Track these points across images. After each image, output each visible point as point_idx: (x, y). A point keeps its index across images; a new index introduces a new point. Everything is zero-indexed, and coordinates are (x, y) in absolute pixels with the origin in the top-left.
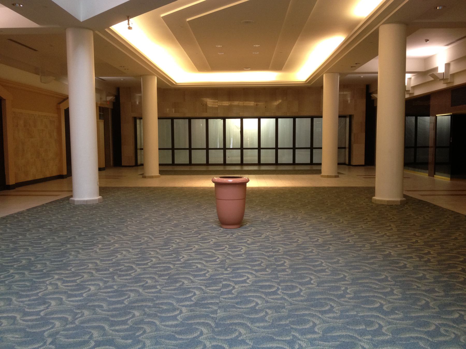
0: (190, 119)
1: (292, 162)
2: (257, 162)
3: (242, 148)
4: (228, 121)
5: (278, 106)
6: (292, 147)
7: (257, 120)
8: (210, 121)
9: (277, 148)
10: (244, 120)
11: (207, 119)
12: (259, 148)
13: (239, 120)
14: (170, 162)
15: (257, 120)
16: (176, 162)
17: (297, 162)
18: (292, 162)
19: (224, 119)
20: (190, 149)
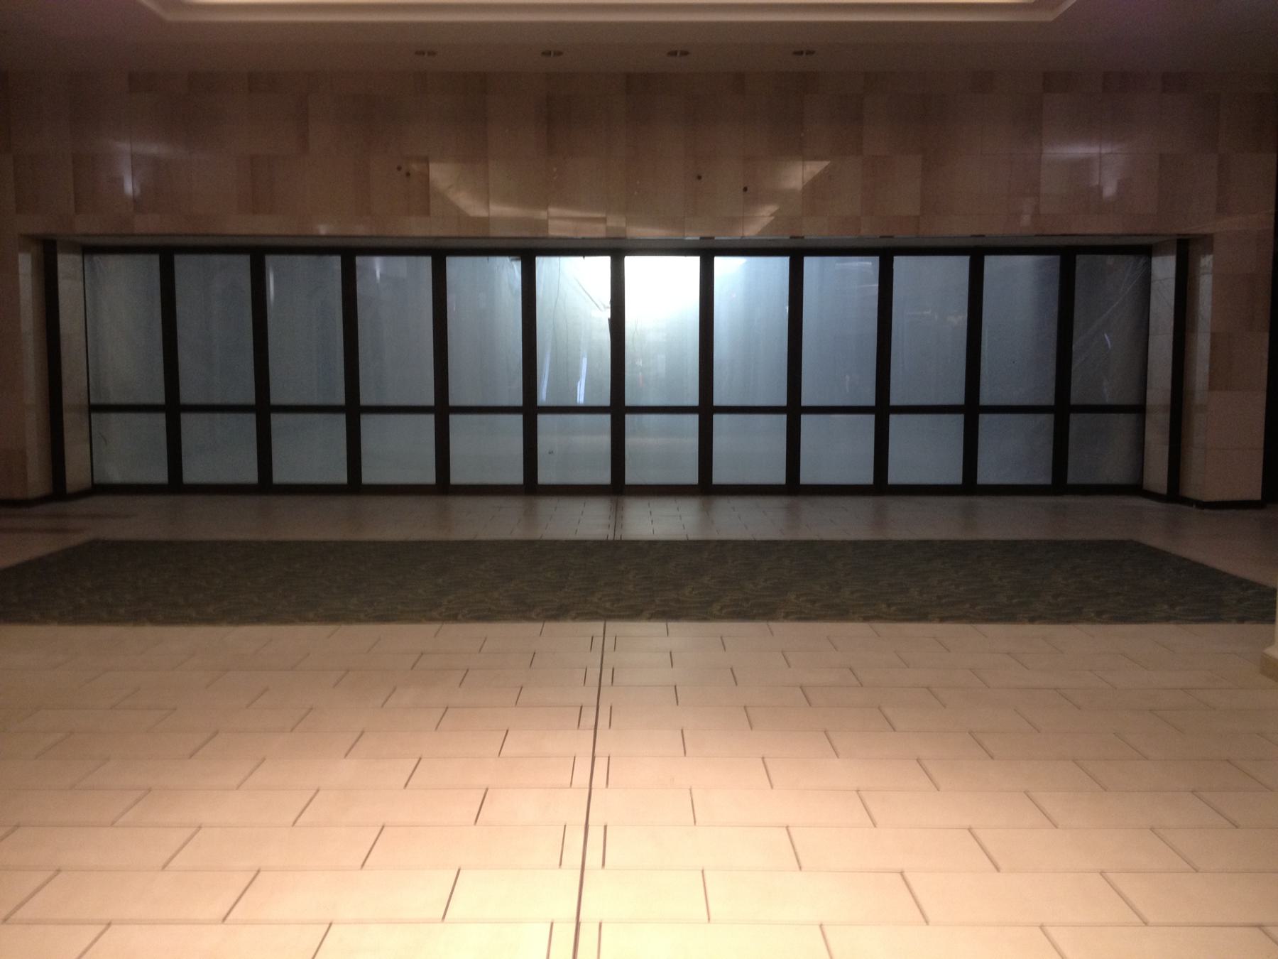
0: (349, 254)
1: (177, 258)
2: (692, 477)
3: (618, 409)
4: (544, 265)
5: (814, 188)
6: (870, 401)
7: (694, 262)
8: (455, 266)
9: (794, 410)
10: (630, 262)
11: (439, 255)
12: (706, 409)
13: (605, 262)
14: (250, 475)
15: (694, 262)
16: (279, 477)
17: (894, 477)
18: (177, 258)
19: (527, 257)
20: (353, 410)
